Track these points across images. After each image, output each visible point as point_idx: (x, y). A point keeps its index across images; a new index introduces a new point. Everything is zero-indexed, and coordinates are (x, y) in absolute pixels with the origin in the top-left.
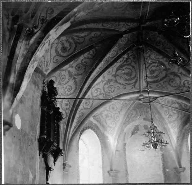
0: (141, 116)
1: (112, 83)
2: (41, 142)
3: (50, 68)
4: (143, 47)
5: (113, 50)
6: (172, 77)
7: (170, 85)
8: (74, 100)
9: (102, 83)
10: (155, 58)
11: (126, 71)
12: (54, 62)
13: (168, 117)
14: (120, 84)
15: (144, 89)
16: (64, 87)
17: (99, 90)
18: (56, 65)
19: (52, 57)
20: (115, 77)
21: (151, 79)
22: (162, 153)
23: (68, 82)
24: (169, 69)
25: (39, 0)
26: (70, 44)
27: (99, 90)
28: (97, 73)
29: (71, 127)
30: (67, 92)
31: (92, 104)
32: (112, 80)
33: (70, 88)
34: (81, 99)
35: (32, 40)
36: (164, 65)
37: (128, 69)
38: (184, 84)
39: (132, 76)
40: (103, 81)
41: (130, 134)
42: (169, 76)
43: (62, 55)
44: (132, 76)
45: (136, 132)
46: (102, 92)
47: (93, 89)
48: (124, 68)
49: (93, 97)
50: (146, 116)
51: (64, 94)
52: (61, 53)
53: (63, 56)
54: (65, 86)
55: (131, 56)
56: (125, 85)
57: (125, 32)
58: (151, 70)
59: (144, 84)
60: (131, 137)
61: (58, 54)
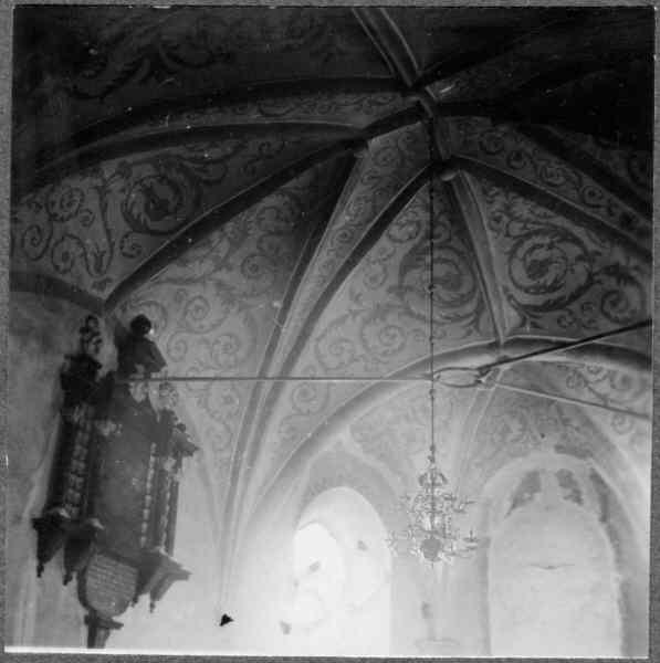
0: (543, 436)
1: (391, 318)
3: (118, 271)
4: (458, 180)
5: (352, 197)
6: (611, 283)
7: (607, 315)
8: (255, 381)
9: (354, 317)
10: (532, 212)
12: (124, 254)
13: (632, 441)
15: (510, 335)
16: (206, 341)
18: (137, 264)
19: (116, 239)
20: (401, 296)
21: (532, 297)
22: (620, 577)
23: (220, 321)
24: (598, 253)
25: (659, 106)
26: (176, 189)
27: (344, 345)
28: (322, 285)
29: (247, 480)
30: (222, 358)
31: (328, 396)
32: (389, 307)
33: (233, 341)
34: (279, 378)
36: (577, 241)
37: (446, 261)
39: (464, 290)
41: (507, 504)
42: (599, 282)
43: (152, 228)
44: (464, 290)
45: (527, 495)
46: (360, 351)
47: (323, 341)
49: (327, 370)
50: (564, 437)
51: (212, 363)
52: (149, 223)
53: (153, 233)
54: (211, 336)
55: (441, 213)
56: (443, 324)
57: (376, 129)
58: (529, 259)
59: (510, 317)
60: (509, 514)
61: (136, 226)
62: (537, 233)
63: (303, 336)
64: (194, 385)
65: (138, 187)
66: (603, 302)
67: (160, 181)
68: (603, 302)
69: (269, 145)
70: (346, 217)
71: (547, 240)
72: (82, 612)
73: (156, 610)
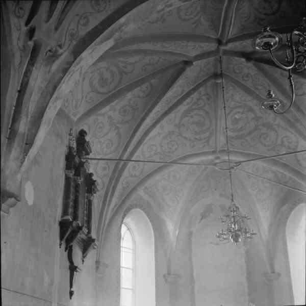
2: (63, 225)
3: (82, 110)
6: (264, 130)
8: (116, 161)
11: (196, 119)
12: (86, 101)
14: (186, 138)
16: (100, 142)
17: (154, 148)
29: (109, 205)
35: (55, 66)
38: (282, 142)
40: (159, 134)
41: (200, 217)
46: (159, 150)
48: (192, 113)
54: (102, 140)
57: (199, 57)
59: (222, 140)
62: (240, 107)
63: (140, 142)
64: (93, 161)
65: (98, 71)
66: (260, 137)
67: (107, 70)
68: (260, 137)
69: (154, 59)
70: (172, 94)
71: (241, 110)
72: (68, 264)
73: (84, 263)
